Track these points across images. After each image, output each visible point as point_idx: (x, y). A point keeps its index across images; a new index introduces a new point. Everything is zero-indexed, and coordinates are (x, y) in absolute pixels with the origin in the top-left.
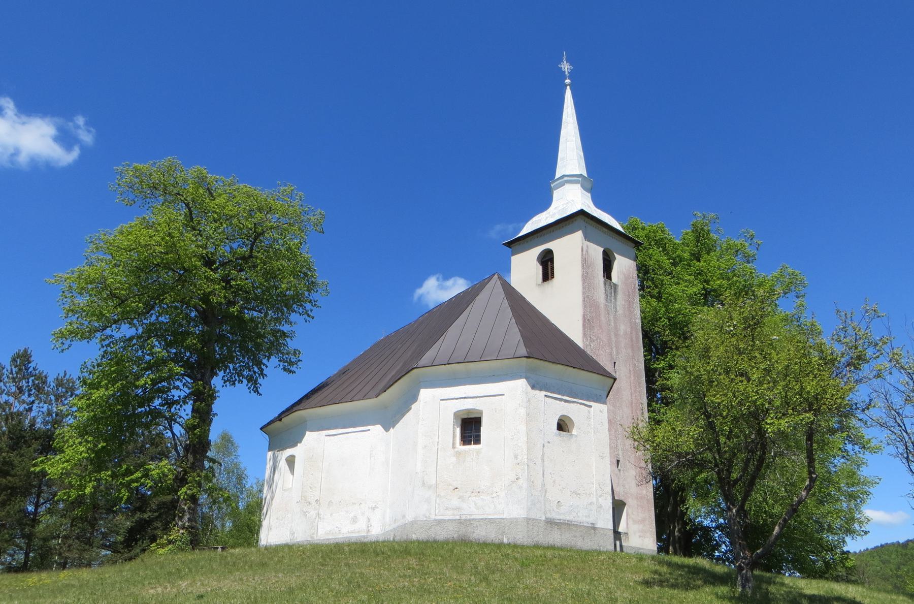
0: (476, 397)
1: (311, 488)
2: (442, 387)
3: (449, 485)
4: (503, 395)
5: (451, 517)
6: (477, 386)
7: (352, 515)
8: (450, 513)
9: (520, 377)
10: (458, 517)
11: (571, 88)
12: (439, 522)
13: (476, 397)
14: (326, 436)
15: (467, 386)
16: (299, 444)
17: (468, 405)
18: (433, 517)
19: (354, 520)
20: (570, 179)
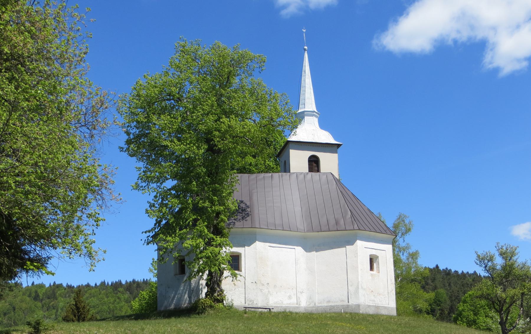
0: (376, 249)
1: (263, 276)
2: (365, 241)
3: (370, 289)
4: (365, 248)
5: (372, 305)
6: (376, 244)
7: (288, 294)
8: (371, 302)
9: (390, 244)
10: (375, 305)
11: (307, 52)
12: (369, 306)
13: (376, 249)
14: (269, 246)
15: (373, 243)
16: (460, 272)
17: (374, 252)
18: (367, 304)
19: (290, 297)
20: (311, 114)
